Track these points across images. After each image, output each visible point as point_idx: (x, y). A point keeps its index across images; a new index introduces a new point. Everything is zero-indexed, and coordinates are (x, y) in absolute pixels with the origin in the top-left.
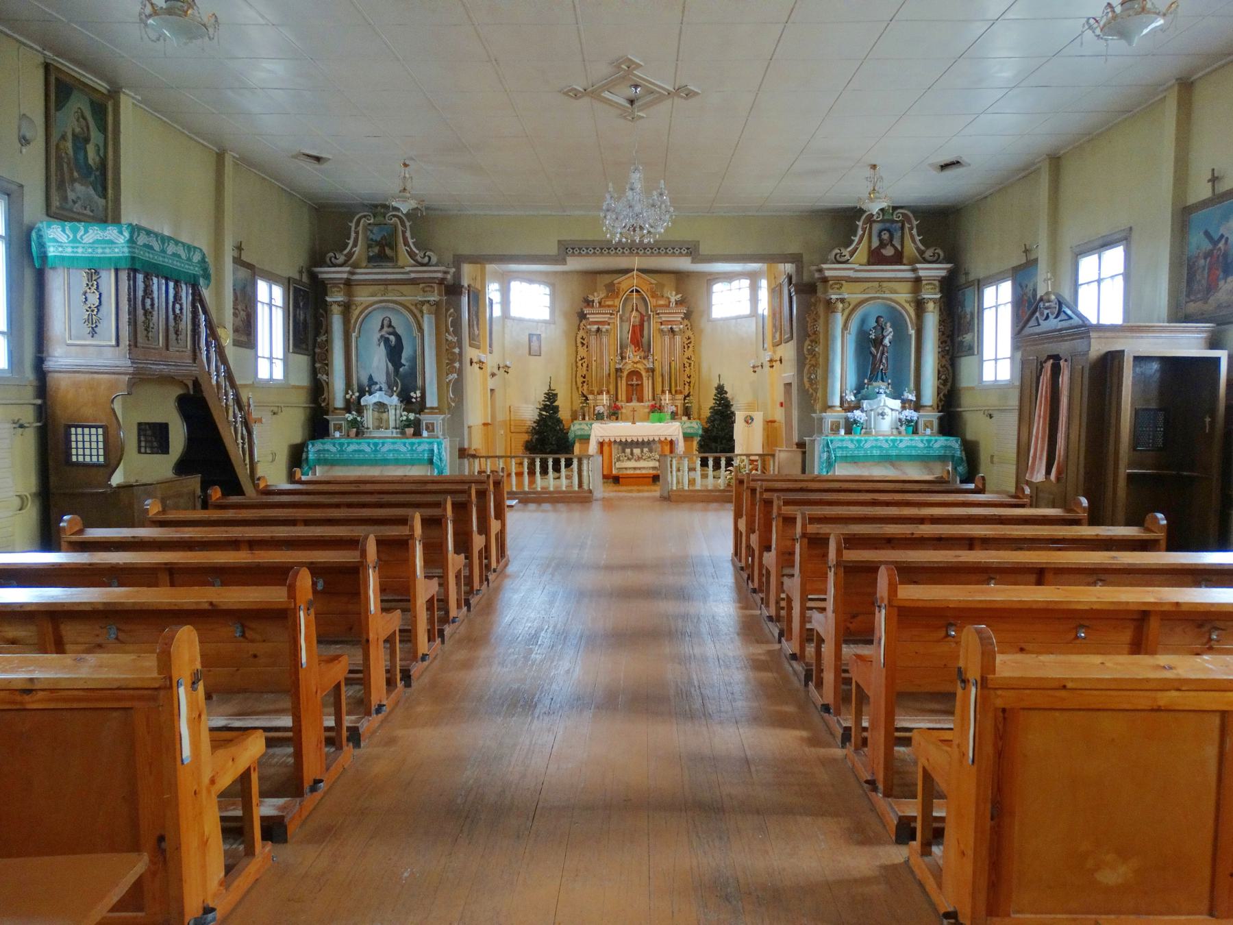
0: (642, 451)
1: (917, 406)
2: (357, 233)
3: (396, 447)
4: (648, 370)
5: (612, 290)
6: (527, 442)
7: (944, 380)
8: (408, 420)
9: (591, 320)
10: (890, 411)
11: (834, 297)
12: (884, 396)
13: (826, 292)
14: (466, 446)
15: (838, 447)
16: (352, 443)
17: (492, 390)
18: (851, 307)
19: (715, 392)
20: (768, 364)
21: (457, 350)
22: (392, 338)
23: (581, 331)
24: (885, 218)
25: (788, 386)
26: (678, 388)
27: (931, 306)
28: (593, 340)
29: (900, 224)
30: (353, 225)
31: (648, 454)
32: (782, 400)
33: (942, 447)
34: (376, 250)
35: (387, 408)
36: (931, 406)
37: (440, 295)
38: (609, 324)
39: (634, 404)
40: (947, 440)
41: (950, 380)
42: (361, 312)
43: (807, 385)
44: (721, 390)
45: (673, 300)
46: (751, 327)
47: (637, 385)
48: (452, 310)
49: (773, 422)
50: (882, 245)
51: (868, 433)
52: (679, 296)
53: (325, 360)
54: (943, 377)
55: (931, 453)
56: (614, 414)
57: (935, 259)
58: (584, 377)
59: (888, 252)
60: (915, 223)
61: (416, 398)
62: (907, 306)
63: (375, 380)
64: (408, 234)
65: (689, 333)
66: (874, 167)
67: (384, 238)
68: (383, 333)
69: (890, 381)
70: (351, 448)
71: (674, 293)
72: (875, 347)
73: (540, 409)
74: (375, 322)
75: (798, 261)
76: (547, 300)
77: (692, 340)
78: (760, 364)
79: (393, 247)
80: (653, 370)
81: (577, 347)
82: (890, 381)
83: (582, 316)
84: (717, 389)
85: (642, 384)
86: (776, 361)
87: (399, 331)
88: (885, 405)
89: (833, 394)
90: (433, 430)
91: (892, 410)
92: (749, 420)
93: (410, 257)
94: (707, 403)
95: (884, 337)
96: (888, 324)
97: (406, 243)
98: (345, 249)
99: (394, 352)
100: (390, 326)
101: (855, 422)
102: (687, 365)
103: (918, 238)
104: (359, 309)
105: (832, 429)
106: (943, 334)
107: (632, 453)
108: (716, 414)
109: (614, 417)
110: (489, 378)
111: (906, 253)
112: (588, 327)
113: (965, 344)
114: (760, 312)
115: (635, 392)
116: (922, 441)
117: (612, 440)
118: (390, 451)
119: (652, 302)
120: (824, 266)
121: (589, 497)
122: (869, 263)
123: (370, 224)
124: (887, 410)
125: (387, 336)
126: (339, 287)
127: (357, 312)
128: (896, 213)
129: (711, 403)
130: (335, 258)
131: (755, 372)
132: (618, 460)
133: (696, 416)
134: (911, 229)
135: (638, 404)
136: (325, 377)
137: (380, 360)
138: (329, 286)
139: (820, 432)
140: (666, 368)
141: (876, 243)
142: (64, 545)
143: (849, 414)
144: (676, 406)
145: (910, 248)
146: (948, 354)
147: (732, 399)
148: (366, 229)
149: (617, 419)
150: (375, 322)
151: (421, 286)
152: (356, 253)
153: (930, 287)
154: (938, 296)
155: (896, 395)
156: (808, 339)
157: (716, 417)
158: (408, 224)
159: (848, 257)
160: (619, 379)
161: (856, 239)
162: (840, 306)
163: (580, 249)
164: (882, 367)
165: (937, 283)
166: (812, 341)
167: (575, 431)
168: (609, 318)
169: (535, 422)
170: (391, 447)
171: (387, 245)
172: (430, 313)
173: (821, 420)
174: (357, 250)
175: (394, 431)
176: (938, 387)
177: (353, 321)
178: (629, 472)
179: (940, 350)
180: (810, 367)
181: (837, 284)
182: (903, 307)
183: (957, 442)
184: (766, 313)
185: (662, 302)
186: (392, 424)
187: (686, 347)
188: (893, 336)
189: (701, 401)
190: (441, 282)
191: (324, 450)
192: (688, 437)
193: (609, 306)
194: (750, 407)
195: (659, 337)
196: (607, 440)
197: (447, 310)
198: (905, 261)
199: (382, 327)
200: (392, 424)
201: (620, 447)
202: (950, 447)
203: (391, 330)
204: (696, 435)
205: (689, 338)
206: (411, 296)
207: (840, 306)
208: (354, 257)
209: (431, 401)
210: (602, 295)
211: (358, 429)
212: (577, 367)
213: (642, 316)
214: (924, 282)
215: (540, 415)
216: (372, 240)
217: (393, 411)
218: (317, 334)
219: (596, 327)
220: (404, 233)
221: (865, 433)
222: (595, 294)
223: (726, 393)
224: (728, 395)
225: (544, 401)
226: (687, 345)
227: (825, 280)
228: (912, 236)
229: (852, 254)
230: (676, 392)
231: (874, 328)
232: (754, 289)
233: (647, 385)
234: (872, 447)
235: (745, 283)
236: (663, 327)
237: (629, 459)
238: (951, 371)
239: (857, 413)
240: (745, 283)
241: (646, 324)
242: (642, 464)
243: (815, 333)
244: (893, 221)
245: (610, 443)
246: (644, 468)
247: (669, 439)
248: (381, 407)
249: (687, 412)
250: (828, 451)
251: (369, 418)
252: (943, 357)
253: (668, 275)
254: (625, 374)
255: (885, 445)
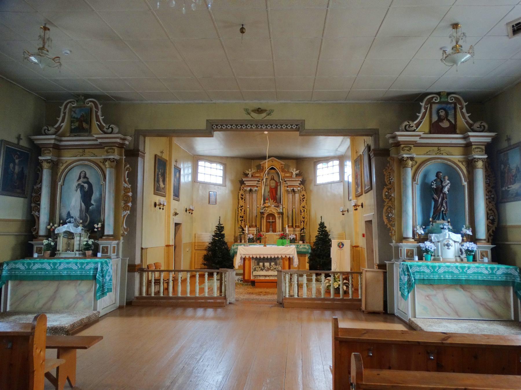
0: (270, 265)
1: (473, 239)
2: (65, 113)
3: (70, 266)
4: (279, 213)
5: (260, 168)
6: (205, 255)
7: (491, 220)
8: (87, 244)
9: (246, 184)
10: (453, 243)
11: (405, 156)
12: (447, 231)
13: (398, 153)
14: (138, 262)
15: (418, 272)
16: (37, 263)
17: (177, 225)
18: (417, 164)
19: (318, 227)
20: (353, 208)
21: (130, 194)
22: (86, 185)
23: (241, 191)
24: (442, 100)
25: (369, 223)
26: (297, 224)
27: (480, 164)
28: (248, 196)
29: (453, 105)
30: (62, 108)
31: (274, 267)
32: (364, 233)
33: (503, 274)
34: (77, 124)
35: (74, 236)
36: (485, 240)
37: (121, 155)
38: (257, 187)
39: (271, 233)
40: (508, 268)
41: (496, 220)
42: (66, 167)
43: (386, 221)
44: (322, 226)
45: (294, 173)
46: (340, 190)
47: (273, 222)
48: (128, 166)
49: (357, 246)
50: (440, 119)
51: (436, 260)
52: (298, 171)
53: (38, 201)
54: (491, 218)
55: (495, 278)
56: (258, 239)
57: (481, 130)
58: (243, 217)
59: (445, 124)
60: (465, 104)
61: (97, 228)
62: (460, 164)
63: (72, 215)
64: (99, 113)
65: (303, 193)
66: (455, 26)
67: (82, 116)
68: (80, 182)
69: (449, 220)
70: (37, 266)
71: (295, 169)
72: (436, 194)
73: (213, 236)
74: (76, 173)
75: (376, 134)
76: (221, 173)
77: (305, 196)
78: (347, 210)
79: (90, 123)
80: (282, 214)
81: (239, 200)
82: (449, 220)
83: (242, 183)
84: (320, 225)
85: (275, 221)
86: (359, 206)
87: (91, 181)
88: (449, 238)
89: (407, 227)
90: (107, 252)
91: (455, 242)
92: (341, 245)
93: (100, 129)
94: (314, 233)
95: (443, 187)
96: (447, 178)
97: (98, 120)
98: (56, 124)
99: (86, 196)
100: (85, 177)
101: (427, 251)
102: (302, 211)
103: (467, 115)
104: (65, 165)
105: (407, 256)
106: (489, 186)
107: (264, 266)
108: (320, 240)
109: (258, 241)
110: (172, 216)
111: (459, 124)
112: (245, 188)
113: (510, 192)
114: (346, 179)
115: (271, 226)
116: (486, 268)
117: (251, 256)
118: (65, 269)
119: (281, 174)
120: (397, 133)
121: (223, 303)
122: (430, 133)
123: (74, 107)
124: (451, 242)
125: (83, 184)
126: (50, 150)
127: (63, 168)
128: (449, 97)
129: (316, 233)
130: (48, 130)
131: (343, 214)
132: (255, 270)
133: (308, 241)
134: (461, 108)
135: (273, 233)
136: (37, 213)
137: (76, 201)
138: (43, 149)
139: (397, 258)
140: (290, 212)
141: (435, 118)
142: (136, 270)
143: (422, 245)
144: (296, 235)
145: (462, 122)
146: (493, 201)
147: (330, 231)
148: (71, 110)
149: (260, 242)
150: (76, 173)
151: (106, 148)
152: (63, 127)
153: (479, 150)
154: (486, 156)
155: (456, 230)
156: (386, 187)
157: (320, 242)
158: (100, 107)
159: (414, 128)
160: (262, 218)
161: (421, 115)
162: (410, 163)
163: (222, 125)
164: (443, 209)
165: (483, 147)
166: (389, 189)
167: (234, 249)
168: (257, 183)
169: (210, 244)
170: (66, 266)
171: (84, 121)
172: (111, 167)
173: (397, 248)
174: (64, 124)
175: (77, 253)
176: (488, 225)
177: (59, 174)
178: (262, 278)
179: (487, 197)
180: (388, 208)
181: (407, 147)
182: (458, 166)
183: (516, 270)
184: (350, 180)
185: (288, 175)
186: (76, 247)
187: (302, 201)
188: (450, 186)
189: (311, 232)
190: (121, 146)
191: (15, 269)
192: (300, 254)
193: (257, 177)
194: (341, 236)
195: (286, 194)
196: (247, 257)
197: (125, 166)
198: (458, 131)
199: (80, 178)
200: (76, 247)
201: (256, 262)
202: (511, 274)
203: (85, 180)
204: (307, 252)
205: (304, 195)
206: (100, 155)
207: (410, 163)
208: (61, 130)
209: (109, 230)
210: (253, 171)
211: (53, 252)
212: (238, 211)
213: (276, 183)
214: (474, 147)
215: (213, 239)
216: (74, 118)
217: (78, 238)
218: (35, 183)
219: (249, 188)
220: (96, 112)
221: (434, 260)
222: (250, 170)
223: (326, 227)
224: (327, 229)
225: (216, 231)
226: (302, 199)
227: (398, 144)
228: (463, 114)
229: (418, 125)
230: (296, 226)
231: (435, 180)
232: (342, 167)
233: (279, 222)
234: (445, 272)
235: (337, 162)
236: (288, 188)
237: (262, 270)
238: (496, 213)
239: (428, 244)
240: (337, 162)
241: (279, 187)
242: (270, 273)
243: (390, 183)
244: (448, 103)
245: (250, 259)
246: (271, 276)
247: (288, 257)
248: (70, 235)
249: (302, 239)
250: (408, 275)
251: (61, 243)
252: (490, 202)
253: (291, 160)
254: (265, 215)
255: (456, 271)
